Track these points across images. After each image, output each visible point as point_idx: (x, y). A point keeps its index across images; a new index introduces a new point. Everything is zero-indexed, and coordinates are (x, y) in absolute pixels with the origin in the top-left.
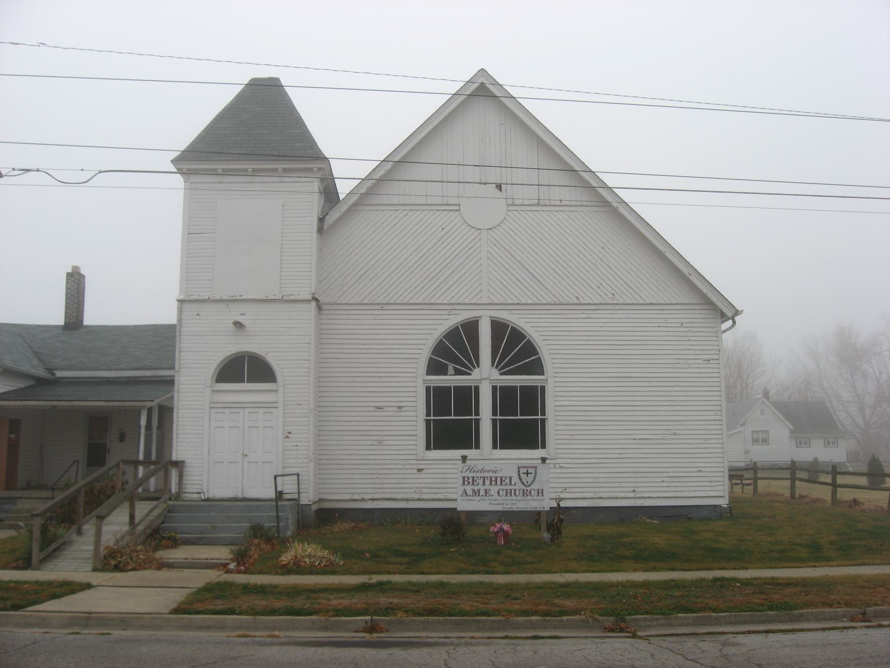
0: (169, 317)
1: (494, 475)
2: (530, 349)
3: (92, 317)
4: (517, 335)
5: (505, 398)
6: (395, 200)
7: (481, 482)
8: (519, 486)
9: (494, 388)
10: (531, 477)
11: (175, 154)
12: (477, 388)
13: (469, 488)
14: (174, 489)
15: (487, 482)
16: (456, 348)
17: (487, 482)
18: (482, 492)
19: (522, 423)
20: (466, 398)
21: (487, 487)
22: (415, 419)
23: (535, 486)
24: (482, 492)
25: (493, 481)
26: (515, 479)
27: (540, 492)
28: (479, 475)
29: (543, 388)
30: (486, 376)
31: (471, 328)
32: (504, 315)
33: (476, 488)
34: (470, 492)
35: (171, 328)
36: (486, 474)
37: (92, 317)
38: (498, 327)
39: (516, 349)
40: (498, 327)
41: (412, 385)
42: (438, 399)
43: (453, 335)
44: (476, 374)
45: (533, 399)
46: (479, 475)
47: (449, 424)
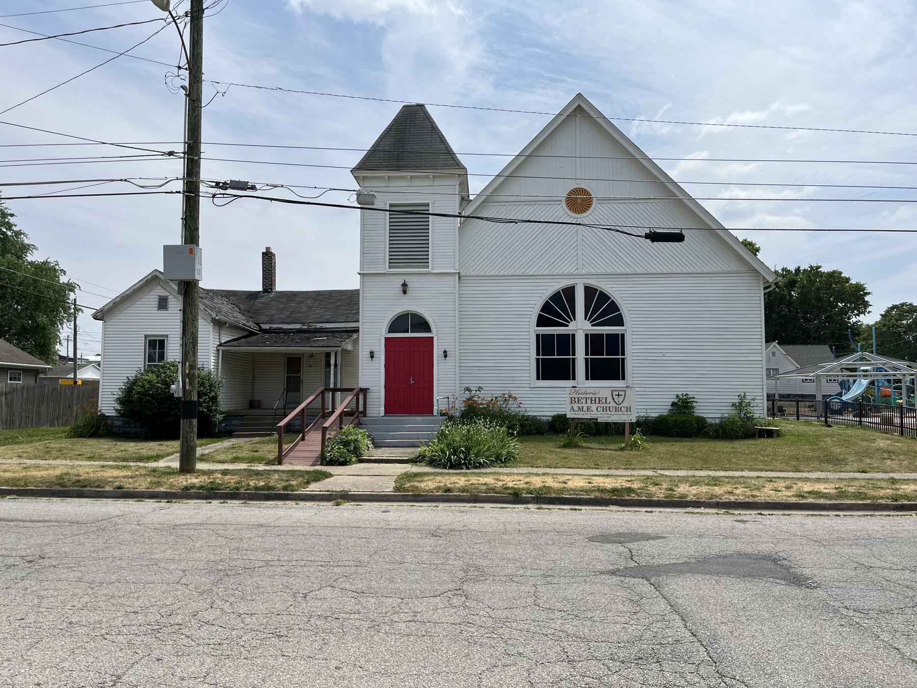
0: (352, 283)
1: (593, 396)
2: (614, 307)
3: (282, 284)
4: (604, 297)
5: (594, 342)
6: (504, 199)
7: (584, 401)
8: (613, 404)
9: (587, 335)
10: (621, 398)
11: (355, 159)
12: (574, 335)
13: (575, 406)
14: (361, 408)
15: (589, 401)
16: (556, 308)
17: (589, 401)
18: (585, 409)
19: (608, 361)
20: (567, 342)
21: (589, 405)
22: (529, 357)
23: (625, 404)
24: (585, 409)
25: (593, 401)
26: (610, 399)
27: (629, 409)
28: (582, 396)
29: (623, 335)
30: (580, 327)
31: (570, 292)
32: (593, 283)
33: (580, 406)
34: (576, 409)
35: (358, 290)
36: (587, 396)
37: (282, 284)
38: (590, 292)
39: (603, 307)
40: (590, 292)
41: (526, 334)
42: (544, 344)
43: (556, 297)
44: (572, 327)
45: (616, 343)
46: (582, 396)
47: (553, 363)
